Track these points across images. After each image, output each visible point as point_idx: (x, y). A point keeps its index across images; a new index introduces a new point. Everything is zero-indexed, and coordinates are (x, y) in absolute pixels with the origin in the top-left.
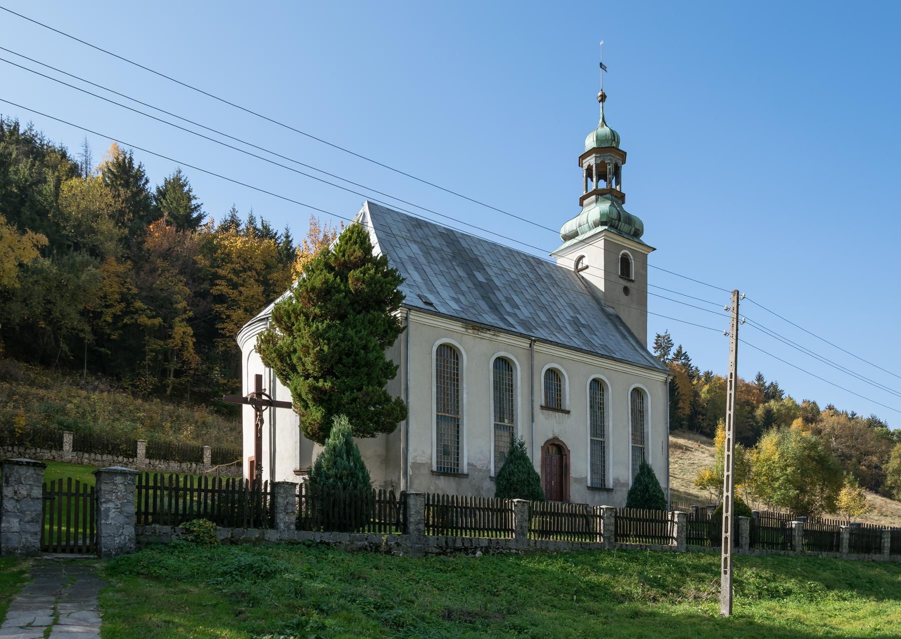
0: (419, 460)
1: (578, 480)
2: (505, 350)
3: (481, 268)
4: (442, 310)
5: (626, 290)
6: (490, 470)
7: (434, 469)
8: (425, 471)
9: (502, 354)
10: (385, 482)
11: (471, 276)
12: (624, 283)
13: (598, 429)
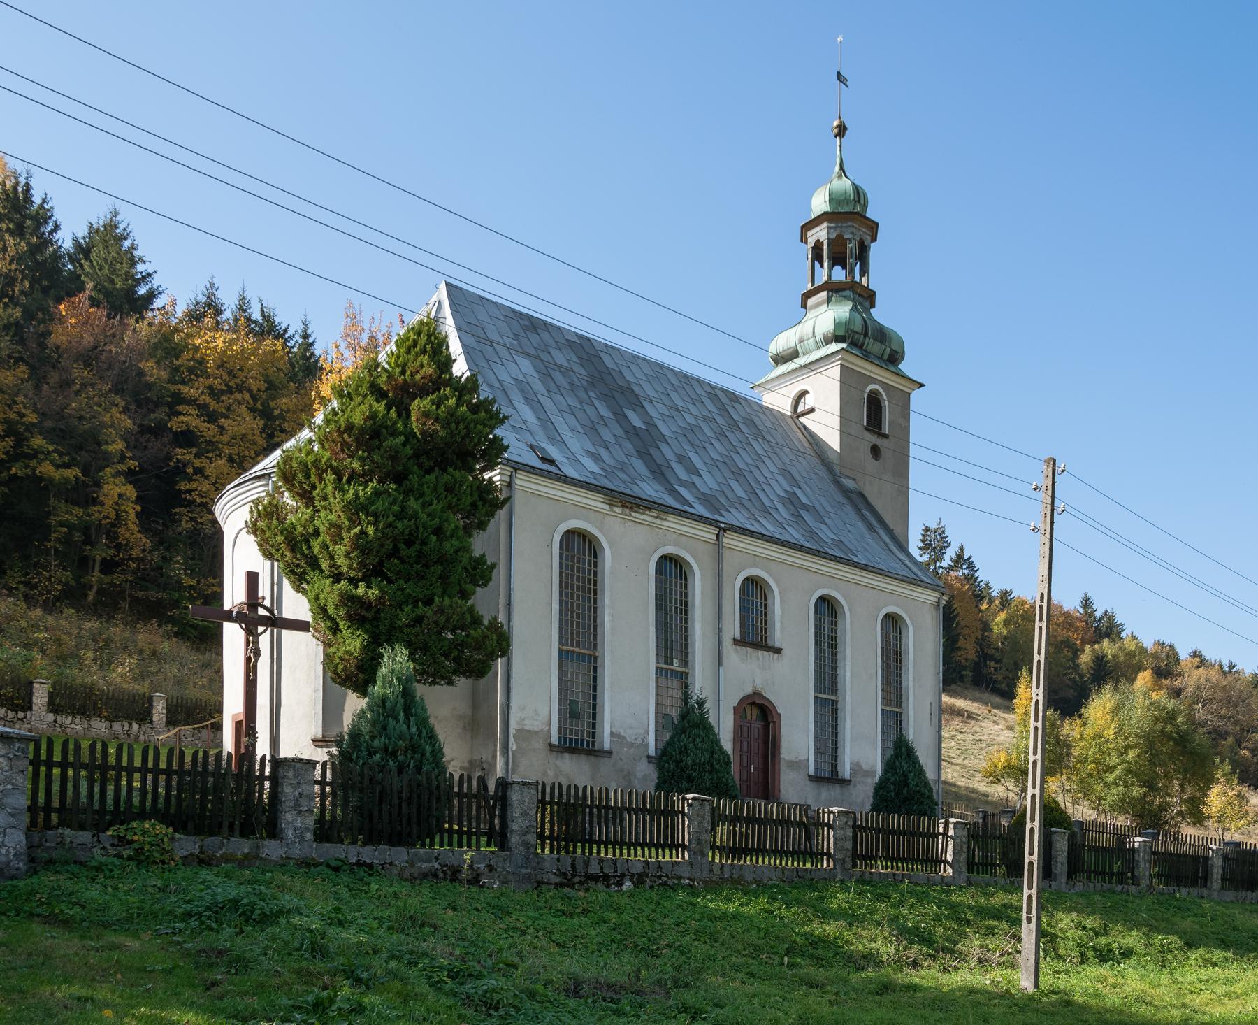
1: (791, 764)
4: (571, 472)
5: (875, 451)
7: (555, 740)
8: (539, 745)
9: (670, 550)
10: (471, 762)
11: (621, 417)
12: (872, 439)
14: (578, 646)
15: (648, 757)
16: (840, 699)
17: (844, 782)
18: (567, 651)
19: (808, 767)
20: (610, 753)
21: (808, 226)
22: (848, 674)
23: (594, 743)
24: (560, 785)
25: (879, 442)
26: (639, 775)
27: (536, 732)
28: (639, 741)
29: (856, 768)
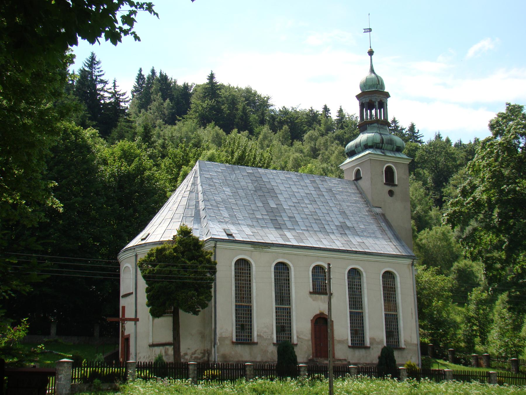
0: (224, 335)
1: (340, 342)
2: (282, 258)
3: (275, 196)
5: (391, 193)
6: (273, 339)
7: (234, 340)
8: (228, 342)
9: (280, 260)
10: (204, 350)
11: (266, 204)
12: (388, 188)
13: (215, 355)
18: (239, 305)
19: (348, 343)
20: (257, 343)
23: (251, 340)
25: (393, 188)
26: (270, 351)
27: (227, 338)
28: (269, 337)
29: (372, 340)
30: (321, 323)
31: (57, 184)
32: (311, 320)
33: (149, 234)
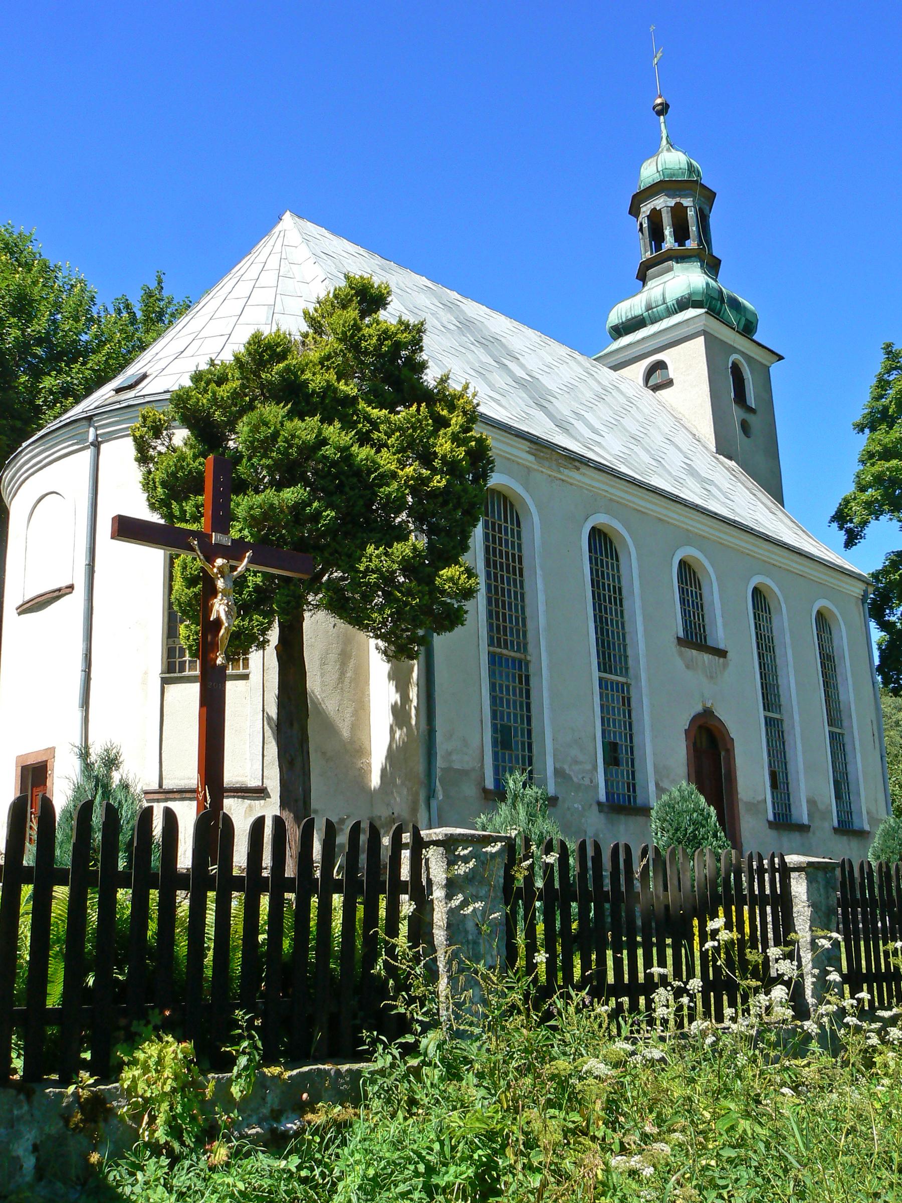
5: (745, 427)
6: (596, 787)
9: (600, 519)
14: (506, 647)
15: (599, 804)
16: (785, 718)
17: (803, 829)
21: (638, 199)
22: (647, 718)
24: (628, 848)
30: (709, 748)
31: (13, 1037)
32: (687, 732)
33: (145, 376)
